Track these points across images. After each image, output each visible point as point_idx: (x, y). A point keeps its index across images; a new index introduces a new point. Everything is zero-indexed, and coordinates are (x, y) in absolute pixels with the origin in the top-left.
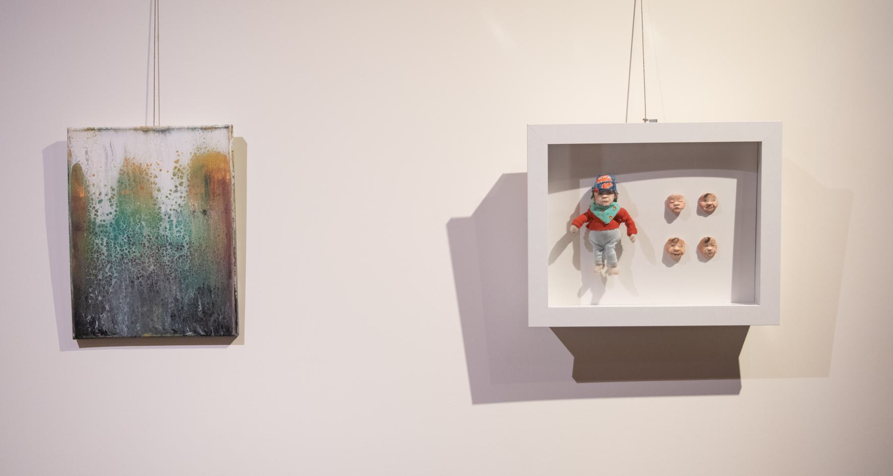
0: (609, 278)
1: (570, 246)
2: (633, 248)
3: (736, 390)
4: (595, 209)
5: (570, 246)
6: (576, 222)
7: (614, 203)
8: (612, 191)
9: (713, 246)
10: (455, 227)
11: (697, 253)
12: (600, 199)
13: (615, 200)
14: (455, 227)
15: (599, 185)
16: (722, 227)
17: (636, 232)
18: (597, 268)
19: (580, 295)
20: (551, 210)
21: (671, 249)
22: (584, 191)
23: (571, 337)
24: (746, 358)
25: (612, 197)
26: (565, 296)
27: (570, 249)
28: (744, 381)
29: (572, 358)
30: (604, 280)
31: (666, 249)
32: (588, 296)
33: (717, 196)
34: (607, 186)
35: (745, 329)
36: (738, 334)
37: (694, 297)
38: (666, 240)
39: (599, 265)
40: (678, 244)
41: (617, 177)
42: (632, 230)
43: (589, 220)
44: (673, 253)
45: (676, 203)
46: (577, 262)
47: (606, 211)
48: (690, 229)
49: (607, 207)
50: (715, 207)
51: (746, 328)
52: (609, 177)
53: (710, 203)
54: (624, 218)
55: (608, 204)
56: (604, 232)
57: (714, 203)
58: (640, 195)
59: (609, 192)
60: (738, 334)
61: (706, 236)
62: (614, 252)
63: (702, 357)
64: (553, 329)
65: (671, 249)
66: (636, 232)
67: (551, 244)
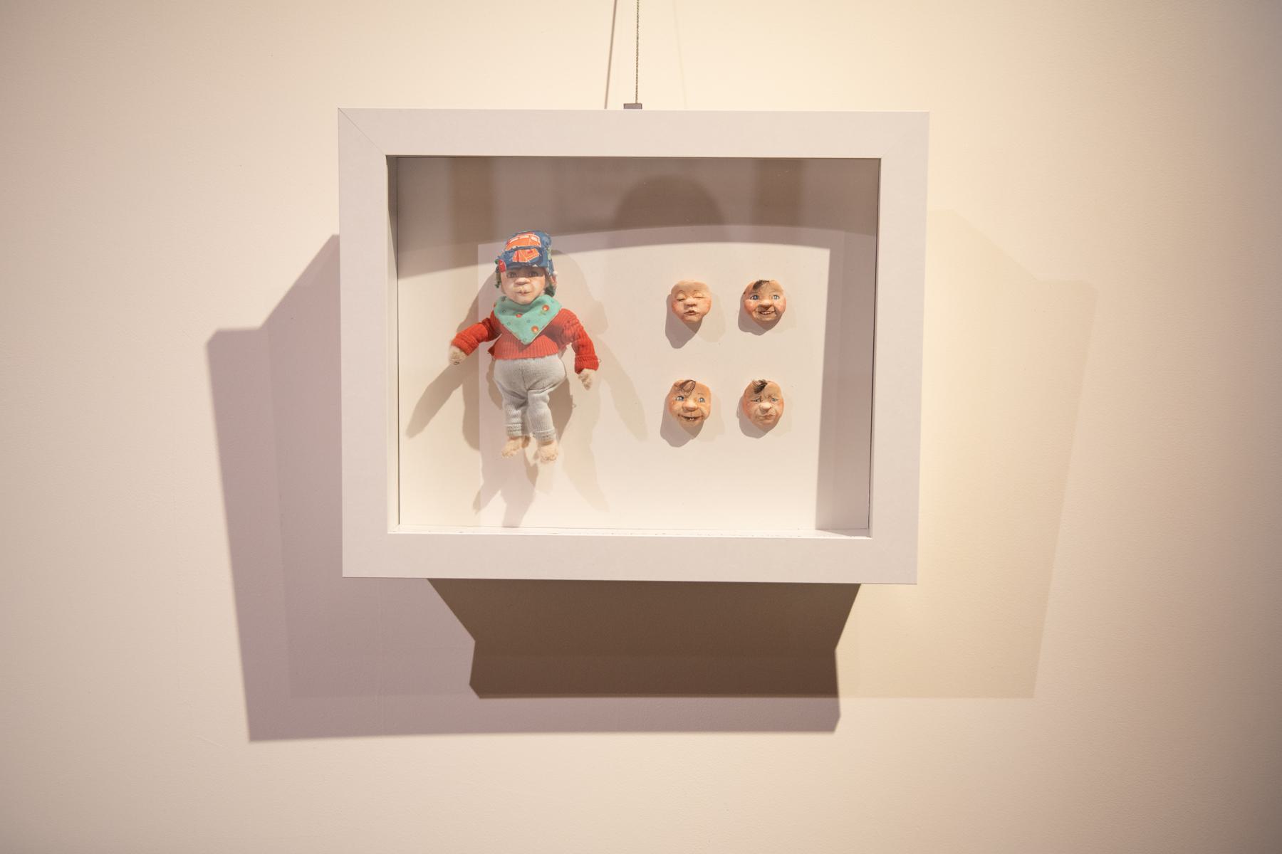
0: (542, 468)
1: (458, 395)
2: (595, 397)
3: (828, 723)
4: (503, 311)
5: (458, 395)
6: (465, 343)
7: (547, 298)
8: (539, 268)
9: (771, 399)
10: (225, 349)
11: (739, 415)
12: (511, 286)
13: (550, 291)
14: (225, 349)
15: (507, 255)
16: (795, 359)
17: (594, 366)
18: (510, 446)
19: (478, 505)
20: (409, 319)
21: (679, 405)
22: (486, 271)
23: (468, 598)
24: (851, 652)
25: (537, 283)
26: (435, 507)
27: (457, 398)
28: (847, 701)
29: (470, 643)
30: (532, 473)
31: (669, 405)
32: (498, 505)
33: (783, 287)
34: (526, 258)
35: (848, 593)
36: (836, 601)
37: (729, 518)
38: (668, 388)
39: (514, 438)
40: (694, 394)
41: (558, 241)
42: (586, 358)
43: (484, 334)
44: (684, 416)
45: (690, 300)
46: (472, 432)
47: (526, 316)
48: (723, 361)
49: (528, 307)
50: (778, 314)
51: (854, 589)
52: (535, 238)
53: (766, 302)
54: (569, 333)
55: (528, 298)
56: (521, 363)
57: (778, 303)
58: (608, 283)
59: (530, 271)
60: (836, 601)
61: (758, 378)
62: (545, 410)
63: (754, 648)
64: (430, 580)
65: (679, 405)
66: (594, 366)
67: (412, 395)
